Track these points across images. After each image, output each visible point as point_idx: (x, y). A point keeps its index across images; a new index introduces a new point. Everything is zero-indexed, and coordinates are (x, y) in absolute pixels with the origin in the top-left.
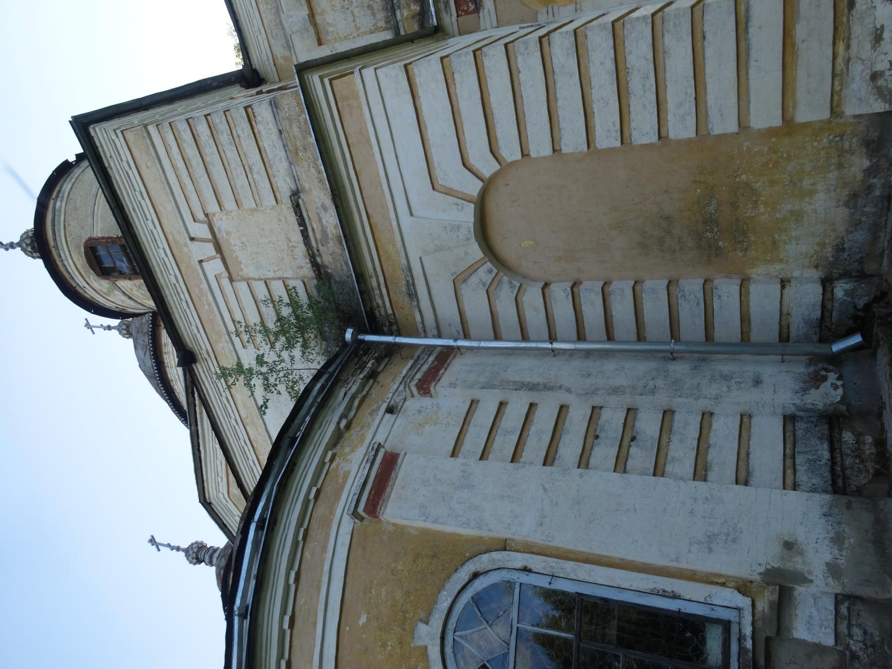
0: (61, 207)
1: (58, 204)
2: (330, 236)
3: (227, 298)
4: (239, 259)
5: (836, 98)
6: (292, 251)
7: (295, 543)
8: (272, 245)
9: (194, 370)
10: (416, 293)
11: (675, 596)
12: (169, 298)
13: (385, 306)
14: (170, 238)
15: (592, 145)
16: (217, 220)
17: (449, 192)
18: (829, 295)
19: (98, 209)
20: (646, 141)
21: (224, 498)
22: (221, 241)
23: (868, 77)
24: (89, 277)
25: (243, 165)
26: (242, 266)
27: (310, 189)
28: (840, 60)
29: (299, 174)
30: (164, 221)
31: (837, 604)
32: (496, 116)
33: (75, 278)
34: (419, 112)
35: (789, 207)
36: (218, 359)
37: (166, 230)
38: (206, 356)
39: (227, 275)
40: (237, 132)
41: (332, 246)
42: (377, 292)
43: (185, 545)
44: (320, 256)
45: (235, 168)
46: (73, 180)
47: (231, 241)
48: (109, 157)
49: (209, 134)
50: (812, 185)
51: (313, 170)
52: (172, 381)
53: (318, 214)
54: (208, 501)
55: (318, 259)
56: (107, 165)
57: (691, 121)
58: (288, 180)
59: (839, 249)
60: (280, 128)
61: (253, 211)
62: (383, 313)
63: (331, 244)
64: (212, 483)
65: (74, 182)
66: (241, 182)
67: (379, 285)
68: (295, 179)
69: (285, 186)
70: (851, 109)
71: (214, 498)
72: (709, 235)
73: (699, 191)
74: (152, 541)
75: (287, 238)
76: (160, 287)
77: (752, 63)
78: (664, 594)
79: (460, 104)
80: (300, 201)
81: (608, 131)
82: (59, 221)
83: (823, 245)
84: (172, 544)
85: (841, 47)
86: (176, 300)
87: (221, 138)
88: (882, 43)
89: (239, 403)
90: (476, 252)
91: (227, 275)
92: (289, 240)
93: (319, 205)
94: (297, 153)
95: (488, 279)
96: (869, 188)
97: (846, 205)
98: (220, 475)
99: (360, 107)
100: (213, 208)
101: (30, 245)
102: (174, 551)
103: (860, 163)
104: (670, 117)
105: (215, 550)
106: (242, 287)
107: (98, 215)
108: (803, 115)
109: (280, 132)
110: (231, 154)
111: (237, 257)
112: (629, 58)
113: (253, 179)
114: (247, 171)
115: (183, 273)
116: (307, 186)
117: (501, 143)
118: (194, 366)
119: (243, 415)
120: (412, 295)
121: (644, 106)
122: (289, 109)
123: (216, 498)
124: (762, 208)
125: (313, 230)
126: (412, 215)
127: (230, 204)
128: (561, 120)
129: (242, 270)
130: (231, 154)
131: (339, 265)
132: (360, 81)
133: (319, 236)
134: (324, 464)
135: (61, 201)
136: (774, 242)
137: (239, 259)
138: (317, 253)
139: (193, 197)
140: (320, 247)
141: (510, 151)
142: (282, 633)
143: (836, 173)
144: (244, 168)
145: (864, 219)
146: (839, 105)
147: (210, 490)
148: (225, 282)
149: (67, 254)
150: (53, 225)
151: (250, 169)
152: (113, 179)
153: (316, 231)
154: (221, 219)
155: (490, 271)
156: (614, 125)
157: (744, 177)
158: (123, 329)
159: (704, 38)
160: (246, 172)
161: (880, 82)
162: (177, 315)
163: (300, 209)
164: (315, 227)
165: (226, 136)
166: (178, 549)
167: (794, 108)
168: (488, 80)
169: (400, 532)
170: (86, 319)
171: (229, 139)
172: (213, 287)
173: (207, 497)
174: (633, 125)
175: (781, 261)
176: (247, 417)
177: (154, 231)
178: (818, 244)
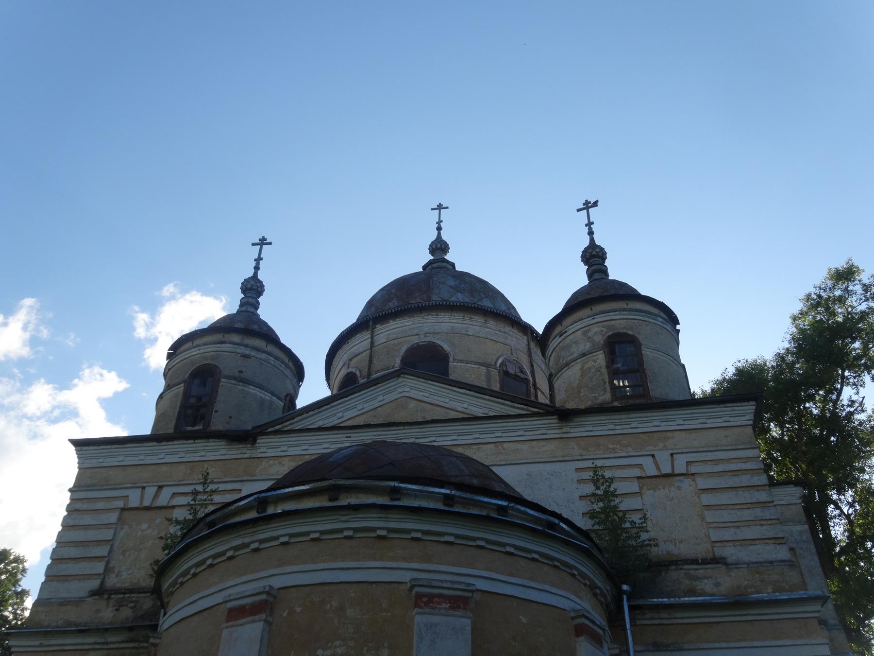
1: (660, 319)
2: (694, 583)
3: (621, 469)
4: (658, 491)
7: (552, 559)
9: (552, 416)
12: (618, 417)
16: (689, 481)
19: (660, 355)
25: (739, 522)
30: (683, 434)
33: (603, 315)
40: (765, 525)
43: (261, 276)
44: (676, 570)
46: (672, 332)
47: (672, 489)
48: (733, 408)
52: (437, 315)
54: (402, 375)
55: (673, 567)
56: (728, 405)
58: (734, 558)
60: (775, 564)
61: (703, 519)
65: (671, 333)
67: (662, 619)
69: (729, 552)
74: (263, 242)
75: (682, 541)
76: (629, 413)
86: (616, 421)
89: (519, 446)
91: (643, 476)
93: (718, 580)
98: (431, 396)
100: (702, 483)
101: (598, 254)
102: (254, 264)
106: (634, 487)
113: (730, 527)
115: (641, 435)
118: (556, 417)
119: (506, 445)
123: (405, 383)
127: (707, 499)
129: (649, 490)
132: (821, 642)
133: (692, 572)
135: (661, 322)
137: (658, 491)
140: (683, 572)
142: (504, 545)
144: (737, 522)
147: (414, 381)
152: (716, 406)
160: (734, 522)
162: (603, 418)
164: (700, 571)
170: (447, 208)
171: (759, 517)
172: (630, 459)
176: (504, 449)
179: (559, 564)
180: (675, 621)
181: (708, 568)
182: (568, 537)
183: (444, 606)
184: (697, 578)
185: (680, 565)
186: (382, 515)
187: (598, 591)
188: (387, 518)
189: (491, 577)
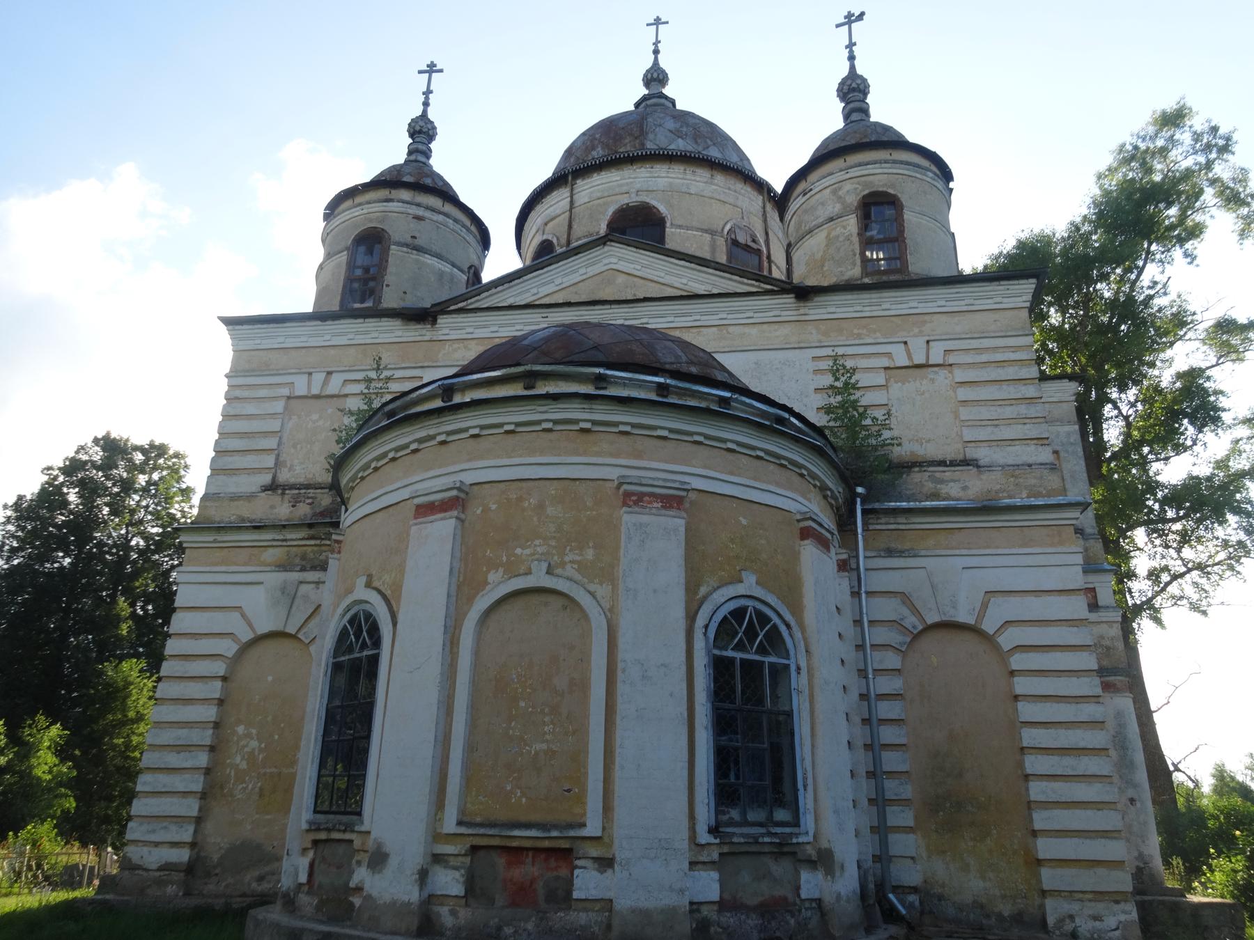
0: (927, 176)
5: (1056, 893)
6: (917, 440)
8: (922, 423)
10: (891, 557)
11: (805, 787)
13: (877, 524)
14: (927, 318)
15: (1023, 725)
17: (985, 605)
18: (907, 891)
20: (1027, 764)
21: (611, 263)
22: (924, 370)
23: (1071, 913)
24: (858, 183)
26: (900, 384)
27: (981, 479)
28: (1081, 896)
29: (995, 473)
31: (815, 900)
32: (1045, 654)
33: (859, 168)
34: (1049, 593)
35: (972, 862)
36: (798, 323)
37: (936, 316)
38: (802, 311)
39: (892, 366)
41: (929, 486)
42: (892, 520)
43: (431, 116)
44: (920, 472)
45: (996, 411)
47: (924, 382)
49: (1027, 396)
50: (990, 879)
51: (998, 487)
53: (959, 481)
54: (608, 243)
57: (1041, 798)
59: (940, 898)
60: (1033, 467)
62: (871, 521)
63: (931, 485)
64: (633, 256)
66: (986, 413)
67: (898, 524)
68: (989, 467)
69: (983, 454)
70: (1049, 903)
71: (611, 251)
72: (948, 805)
73: (983, 799)
74: (432, 69)
77: (1081, 841)
78: (805, 779)
79: (1055, 628)
80: (971, 467)
81: (1035, 739)
82: (917, 172)
83: (943, 886)
84: (431, 96)
85: (1090, 896)
87: (1023, 406)
88: (1092, 921)
89: (747, 330)
90: (932, 618)
92: (929, 441)
93: (967, 484)
94: (1013, 476)
95: (907, 623)
96: (988, 916)
97: (975, 902)
98: (643, 269)
99: (1052, 545)
100: (960, 375)
103: (1006, 909)
104: (1044, 784)
105: (428, 156)
106: (880, 379)
107: (922, 219)
108: (1045, 873)
109: (1030, 465)
110: (1009, 412)
111: (909, 382)
112: (1087, 758)
114: (995, 423)
115: (892, 318)
116: (984, 477)
117: (1024, 656)
118: (792, 296)
119: (731, 329)
120: (890, 553)
121: (1053, 766)
122: (1050, 480)
124: (971, 844)
125: (944, 472)
126: (963, 568)
127: (963, 394)
128: (1042, 704)
130: (1009, 412)
131: (910, 487)
133: (938, 475)
134: (814, 479)
135: (931, 178)
136: (944, 852)
137: (907, 384)
138: (923, 469)
139: (969, 359)
140: (928, 474)
141: (1017, 662)
142: (725, 441)
143: (998, 894)
145: (965, 913)
146: (1051, 895)
148: (885, 362)
149: (886, 171)
150: (908, 163)
151: (996, 426)
153: (943, 474)
154: (946, 378)
155: (914, 627)
156: (1040, 743)
157: (995, 832)
158: (652, 74)
159: (1099, 810)
161: (1068, 921)
162: (849, 297)
163: (964, 465)
164: (947, 474)
165: (1025, 412)
166: (426, 104)
167: (1050, 867)
168: (1073, 653)
169: (796, 556)
170: (667, 23)
173: (613, 244)
174: (1039, 757)
175: (929, 857)
176: (728, 333)
177: (935, 304)
178: (944, 883)
183: (655, 505)
184: (942, 481)
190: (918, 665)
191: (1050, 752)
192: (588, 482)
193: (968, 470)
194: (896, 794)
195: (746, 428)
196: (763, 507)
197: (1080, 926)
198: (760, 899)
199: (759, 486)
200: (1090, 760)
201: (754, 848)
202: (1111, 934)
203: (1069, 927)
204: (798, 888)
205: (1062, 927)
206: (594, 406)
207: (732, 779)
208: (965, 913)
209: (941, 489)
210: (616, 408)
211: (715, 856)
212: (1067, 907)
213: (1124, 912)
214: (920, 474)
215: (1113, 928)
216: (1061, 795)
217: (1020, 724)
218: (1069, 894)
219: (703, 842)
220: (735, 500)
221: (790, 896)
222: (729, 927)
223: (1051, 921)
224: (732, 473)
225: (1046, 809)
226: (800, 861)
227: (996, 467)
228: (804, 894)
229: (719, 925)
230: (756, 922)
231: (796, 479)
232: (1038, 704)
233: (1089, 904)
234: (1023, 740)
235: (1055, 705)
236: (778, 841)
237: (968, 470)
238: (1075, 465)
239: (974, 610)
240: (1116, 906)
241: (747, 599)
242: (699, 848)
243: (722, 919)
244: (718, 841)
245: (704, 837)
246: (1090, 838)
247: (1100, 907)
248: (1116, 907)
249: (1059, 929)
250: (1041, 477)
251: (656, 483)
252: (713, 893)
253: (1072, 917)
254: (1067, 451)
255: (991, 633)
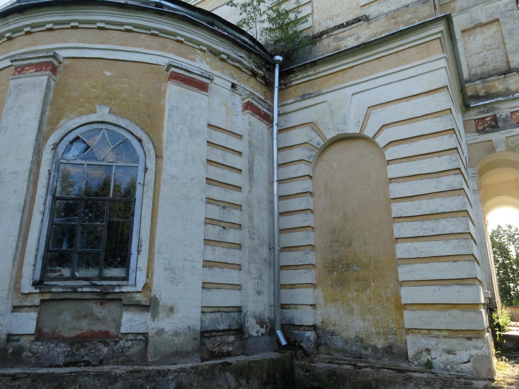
2: (340, 43)
5: (417, 331)
6: (330, 18)
7: (149, 29)
10: (305, 99)
13: (297, 80)
17: (367, 117)
18: (307, 328)
20: (395, 231)
23: (427, 347)
28: (438, 333)
29: (380, 20)
42: (305, 75)
44: (327, 37)
51: (382, 29)
53: (354, 34)
59: (333, 334)
60: (410, 6)
62: (292, 79)
67: (310, 76)
68: (377, 18)
69: (372, 11)
70: (410, 339)
75: (338, 15)
78: (139, 246)
80: (362, 22)
83: (335, 325)
85: (445, 333)
90: (330, 135)
93: (359, 35)
94: (393, 18)
95: (314, 143)
97: (357, 337)
103: (380, 343)
108: (407, 314)
116: (372, 26)
117: (396, 148)
122: (422, 11)
124: (355, 294)
125: (344, 32)
126: (353, 95)
133: (340, 35)
134: (199, 45)
136: (336, 301)
138: (329, 35)
140: (332, 37)
142: (94, 22)
143: (374, 331)
145: (349, 346)
155: (318, 144)
156: (406, 213)
161: (425, 353)
164: (346, 33)
169: (161, 94)
174: (405, 224)
175: (326, 304)
178: (335, 323)
179: (157, 32)
180: (319, 75)
181: (353, 28)
182: (174, 11)
183: (31, 71)
184: (343, 39)
185: (330, 32)
186: (5, 22)
187: (224, 56)
188: (8, 23)
189: (78, 46)
190: (324, 170)
191: (414, 219)
192: (7, 69)
193: (361, 25)
194: (301, 261)
195: (127, 12)
196: (130, 63)
197: (435, 358)
198: (78, 332)
199: (126, 49)
200: (448, 221)
201: (74, 296)
202: (463, 366)
203: (424, 358)
204: (118, 325)
205: (419, 358)
206: (9, 21)
207: (64, 247)
208: (349, 346)
209: (341, 45)
210: (19, 17)
211: (37, 302)
212: (423, 342)
213: (476, 348)
214: (328, 39)
215: (465, 360)
216: (422, 252)
217: (391, 200)
218: (427, 332)
219: (26, 292)
220: (102, 61)
221: (113, 331)
222: (38, 352)
223: (411, 353)
224: (102, 43)
225: (409, 264)
226: (125, 305)
227: (382, 15)
228: (123, 330)
229: (30, 351)
230: (65, 349)
231: (150, 39)
232: (405, 183)
233: (444, 340)
234: (393, 212)
235: (419, 182)
236: (98, 290)
237: (361, 25)
238: (512, 25)
239: (359, 122)
240: (468, 342)
241: (100, 124)
242: (24, 296)
243: (33, 347)
244: (38, 291)
245: (27, 287)
246: (446, 285)
247: (453, 343)
248: (468, 343)
249: (417, 360)
250: (416, 11)
251: (31, 56)
252: (31, 328)
253: (428, 350)
254: (506, 17)
255: (371, 136)
